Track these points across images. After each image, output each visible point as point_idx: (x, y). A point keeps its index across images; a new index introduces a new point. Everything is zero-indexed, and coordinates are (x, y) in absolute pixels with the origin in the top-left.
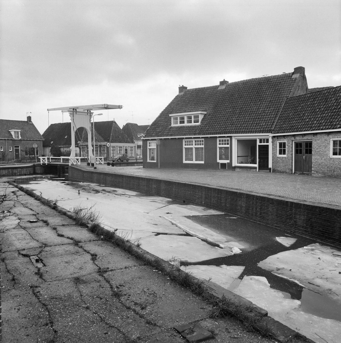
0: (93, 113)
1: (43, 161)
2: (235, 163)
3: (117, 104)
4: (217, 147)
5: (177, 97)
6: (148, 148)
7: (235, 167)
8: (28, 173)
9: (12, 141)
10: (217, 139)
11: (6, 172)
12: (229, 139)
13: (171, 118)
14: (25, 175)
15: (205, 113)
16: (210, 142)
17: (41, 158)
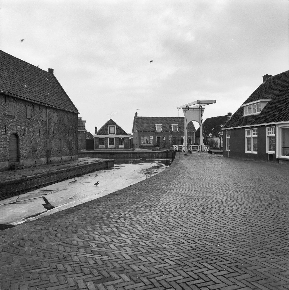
0: (204, 108)
1: (175, 148)
2: (279, 155)
3: (212, 99)
4: (226, 139)
5: (261, 86)
6: (226, 138)
7: (279, 159)
8: (164, 157)
9: (171, 133)
10: (245, 130)
11: (148, 155)
12: (274, 127)
13: (243, 108)
14: (161, 158)
15: (269, 100)
16: (261, 131)
17: (174, 145)
